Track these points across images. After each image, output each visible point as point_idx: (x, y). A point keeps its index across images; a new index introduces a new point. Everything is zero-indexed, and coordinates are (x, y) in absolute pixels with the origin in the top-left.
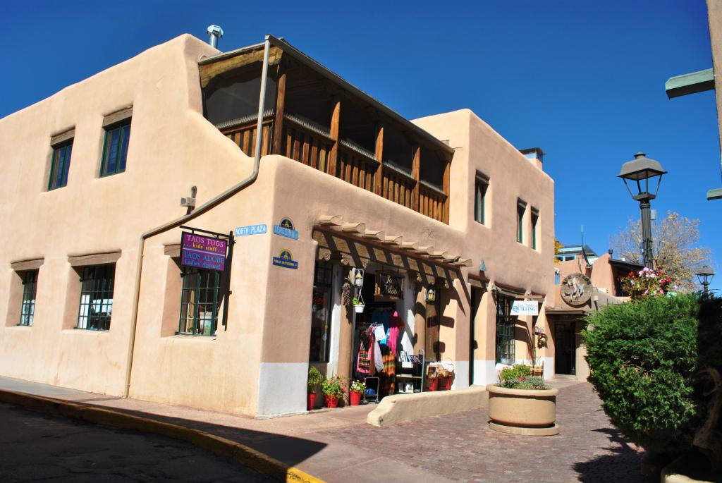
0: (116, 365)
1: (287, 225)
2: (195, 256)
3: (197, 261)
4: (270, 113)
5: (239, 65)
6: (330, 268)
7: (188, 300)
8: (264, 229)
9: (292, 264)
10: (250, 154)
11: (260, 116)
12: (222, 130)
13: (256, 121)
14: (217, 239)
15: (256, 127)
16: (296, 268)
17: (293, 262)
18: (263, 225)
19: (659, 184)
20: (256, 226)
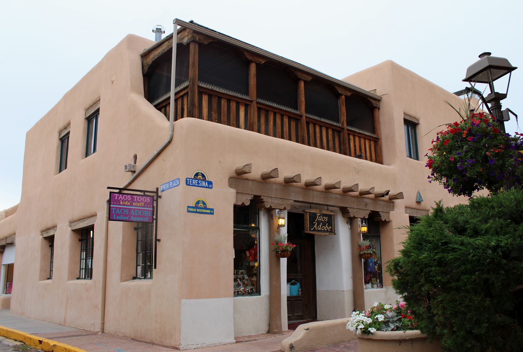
1: (200, 177)
2: (123, 211)
5: (166, 50)
6: (257, 212)
9: (208, 211)
12: (156, 106)
14: (144, 195)
16: (213, 214)
17: (208, 209)
18: (177, 179)
19: (517, 121)
20: (173, 181)
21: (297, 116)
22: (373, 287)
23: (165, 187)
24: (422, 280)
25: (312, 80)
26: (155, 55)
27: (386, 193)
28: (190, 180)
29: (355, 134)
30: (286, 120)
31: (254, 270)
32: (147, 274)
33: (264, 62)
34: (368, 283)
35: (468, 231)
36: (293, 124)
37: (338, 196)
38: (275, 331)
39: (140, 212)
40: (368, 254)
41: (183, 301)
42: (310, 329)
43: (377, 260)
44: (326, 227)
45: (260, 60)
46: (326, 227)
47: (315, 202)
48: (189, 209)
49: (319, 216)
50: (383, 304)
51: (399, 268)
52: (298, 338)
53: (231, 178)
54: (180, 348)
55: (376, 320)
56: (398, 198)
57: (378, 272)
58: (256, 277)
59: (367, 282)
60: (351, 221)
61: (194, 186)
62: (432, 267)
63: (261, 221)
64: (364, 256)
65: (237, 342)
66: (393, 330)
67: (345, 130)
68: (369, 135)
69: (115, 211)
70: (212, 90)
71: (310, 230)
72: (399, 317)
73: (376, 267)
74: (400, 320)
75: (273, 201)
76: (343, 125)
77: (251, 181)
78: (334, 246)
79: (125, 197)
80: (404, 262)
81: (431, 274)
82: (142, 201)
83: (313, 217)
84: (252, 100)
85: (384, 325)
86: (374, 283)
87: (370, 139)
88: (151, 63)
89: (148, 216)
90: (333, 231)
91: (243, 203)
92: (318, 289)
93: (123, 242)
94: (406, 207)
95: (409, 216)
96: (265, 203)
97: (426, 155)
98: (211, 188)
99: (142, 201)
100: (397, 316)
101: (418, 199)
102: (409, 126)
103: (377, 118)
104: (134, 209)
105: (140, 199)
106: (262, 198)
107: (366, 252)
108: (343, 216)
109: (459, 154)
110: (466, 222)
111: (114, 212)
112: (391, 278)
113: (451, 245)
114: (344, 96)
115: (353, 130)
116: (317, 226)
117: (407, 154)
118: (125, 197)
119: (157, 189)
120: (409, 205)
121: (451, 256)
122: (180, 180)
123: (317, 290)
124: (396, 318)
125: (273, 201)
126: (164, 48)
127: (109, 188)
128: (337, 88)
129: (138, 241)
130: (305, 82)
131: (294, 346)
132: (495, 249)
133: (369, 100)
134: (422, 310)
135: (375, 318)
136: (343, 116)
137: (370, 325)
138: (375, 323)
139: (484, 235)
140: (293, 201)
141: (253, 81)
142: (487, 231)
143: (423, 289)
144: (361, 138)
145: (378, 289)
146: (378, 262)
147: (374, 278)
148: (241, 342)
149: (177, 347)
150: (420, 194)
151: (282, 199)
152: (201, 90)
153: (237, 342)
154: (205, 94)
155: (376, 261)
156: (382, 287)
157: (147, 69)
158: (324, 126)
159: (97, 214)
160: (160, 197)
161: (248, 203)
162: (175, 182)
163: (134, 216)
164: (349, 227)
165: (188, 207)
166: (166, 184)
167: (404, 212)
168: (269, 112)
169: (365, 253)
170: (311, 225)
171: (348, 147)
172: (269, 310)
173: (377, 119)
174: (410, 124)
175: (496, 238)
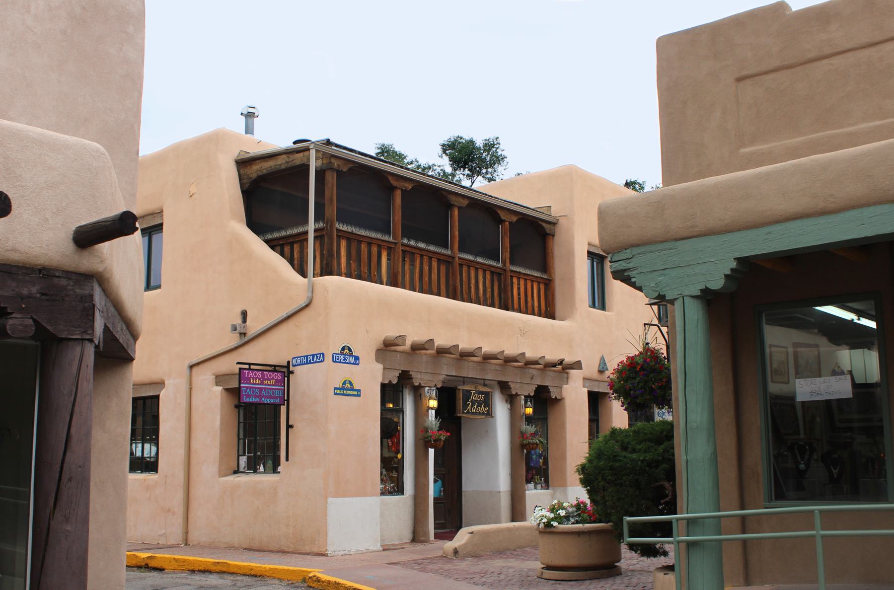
0: (169, 510)
3: (256, 396)
4: (321, 225)
5: (283, 167)
6: (401, 390)
7: (769, 432)
8: (322, 358)
9: (355, 393)
10: (304, 274)
11: (311, 226)
13: (307, 233)
15: (307, 240)
18: (320, 354)
20: (313, 356)
21: (447, 257)
22: (535, 488)
23: (301, 361)
24: (600, 479)
25: (468, 204)
26: (263, 168)
27: (560, 362)
28: (337, 355)
29: (519, 275)
30: (435, 264)
31: (392, 463)
32: (258, 467)
33: (411, 187)
34: (530, 483)
35: (629, 449)
36: (443, 269)
37: (498, 368)
38: (422, 539)
39: (271, 393)
40: (533, 444)
41: (330, 500)
42: (474, 532)
43: (542, 451)
44: (482, 409)
45: (406, 185)
46: (482, 408)
47: (470, 376)
48: (336, 391)
49: (474, 394)
50: (562, 502)
51: (585, 470)
52: (463, 542)
53: (378, 351)
54: (329, 555)
55: (557, 516)
56: (575, 368)
57: (544, 468)
58: (396, 472)
59: (528, 481)
60: (511, 399)
61: (340, 362)
62: (606, 470)
63: (406, 402)
64: (528, 447)
65: (384, 550)
66: (573, 523)
67: (507, 272)
68: (539, 276)
69: (246, 391)
70: (352, 233)
71: (463, 413)
72: (578, 513)
73: (541, 460)
74: (579, 515)
75: (423, 377)
76: (504, 263)
77: (399, 353)
78: (489, 433)
79: (255, 374)
80: (588, 466)
81: (606, 475)
82: (273, 379)
83: (467, 394)
84: (396, 241)
85: (565, 519)
86: (538, 482)
87: (539, 280)
88: (255, 177)
89: (279, 397)
90: (490, 414)
91: (390, 380)
92: (463, 489)
93: (222, 424)
94: (584, 379)
95: (588, 391)
96: (414, 380)
97: (609, 377)
98: (358, 364)
99: (273, 379)
100: (577, 512)
101: (601, 367)
102: (595, 260)
103: (550, 249)
104: (265, 389)
105: (270, 375)
106: (411, 373)
107: (531, 441)
108: (502, 393)
109: (633, 384)
110: (629, 443)
111: (244, 393)
112: (579, 477)
113: (618, 458)
114: (507, 223)
115: (518, 270)
116: (472, 407)
117: (589, 303)
118: (255, 374)
119: (289, 362)
120: (588, 375)
121: (617, 464)
122: (325, 355)
123: (463, 490)
124: (576, 513)
125: (423, 377)
126: (279, 163)
127: (238, 363)
128: (499, 212)
129: (239, 423)
130: (459, 208)
131: (458, 550)
132: (643, 461)
133: (540, 224)
134: (599, 498)
135: (558, 513)
136: (506, 252)
137: (553, 519)
138: (558, 518)
139: (638, 452)
140: (445, 376)
141: (397, 217)
142: (640, 450)
143: (600, 484)
144: (528, 281)
145: (543, 491)
146: (543, 455)
147: (537, 476)
148: (388, 549)
149: (324, 553)
150: (604, 360)
151: (432, 374)
152: (340, 234)
153: (384, 550)
154: (343, 239)
155: (541, 452)
156: (548, 489)
157: (249, 184)
158: (480, 268)
159: (166, 382)
160: (292, 372)
161: (395, 381)
162: (317, 357)
163: (265, 397)
164: (509, 407)
165: (335, 388)
166: (302, 358)
167: (582, 386)
168: (415, 254)
169: (529, 443)
170: (465, 405)
171: (510, 296)
172: (413, 513)
173: (550, 251)
174: (596, 257)
175: (644, 454)
